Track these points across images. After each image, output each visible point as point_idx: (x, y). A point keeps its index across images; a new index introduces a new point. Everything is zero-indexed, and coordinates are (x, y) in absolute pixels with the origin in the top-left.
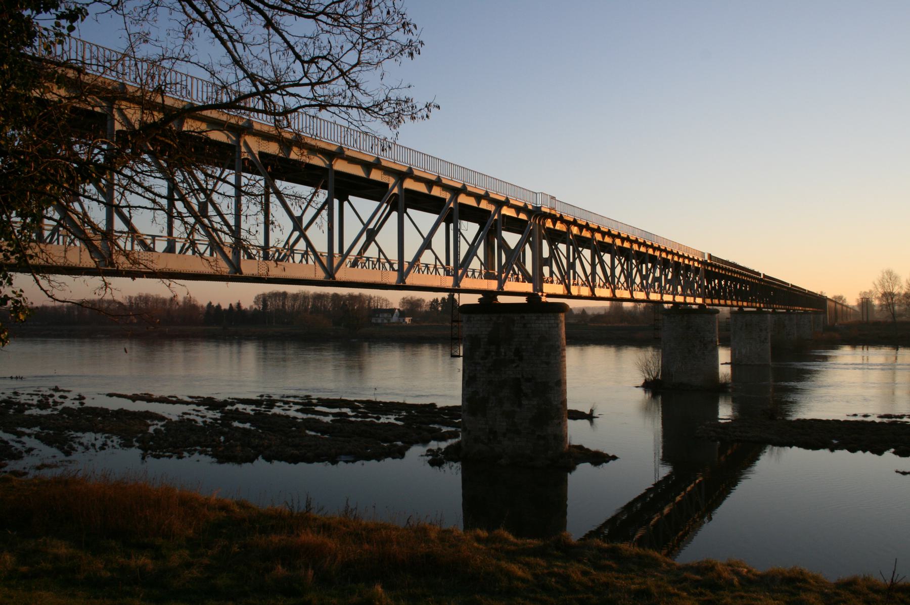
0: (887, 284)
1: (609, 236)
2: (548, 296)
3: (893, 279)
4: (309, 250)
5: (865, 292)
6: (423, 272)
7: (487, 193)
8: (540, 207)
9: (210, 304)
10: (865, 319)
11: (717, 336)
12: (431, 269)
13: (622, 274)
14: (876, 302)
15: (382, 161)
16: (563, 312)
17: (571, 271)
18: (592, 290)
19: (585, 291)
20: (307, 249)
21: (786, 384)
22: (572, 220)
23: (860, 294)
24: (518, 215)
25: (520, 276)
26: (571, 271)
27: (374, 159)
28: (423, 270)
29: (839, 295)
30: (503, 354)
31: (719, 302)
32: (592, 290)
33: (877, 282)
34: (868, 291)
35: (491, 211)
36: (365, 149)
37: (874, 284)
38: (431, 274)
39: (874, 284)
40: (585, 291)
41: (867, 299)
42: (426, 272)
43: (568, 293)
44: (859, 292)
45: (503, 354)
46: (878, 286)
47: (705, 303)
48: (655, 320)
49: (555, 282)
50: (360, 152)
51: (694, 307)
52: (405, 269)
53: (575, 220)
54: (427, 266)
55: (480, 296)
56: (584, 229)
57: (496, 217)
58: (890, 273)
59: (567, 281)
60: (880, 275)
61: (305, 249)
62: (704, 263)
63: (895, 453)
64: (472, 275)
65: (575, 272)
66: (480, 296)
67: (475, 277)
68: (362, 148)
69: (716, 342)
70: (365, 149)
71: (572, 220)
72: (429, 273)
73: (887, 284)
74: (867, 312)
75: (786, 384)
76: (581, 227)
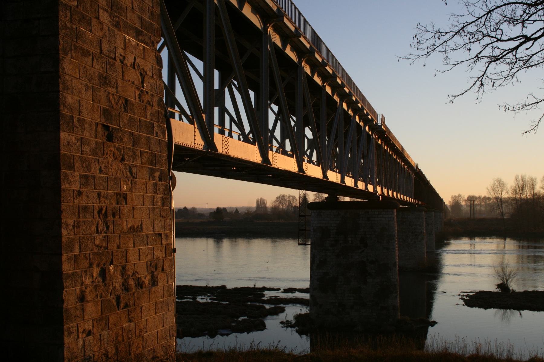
0: (497, 189)
3: (502, 186)
5: (455, 196)
10: (472, 217)
13: (233, 123)
14: (463, 203)
17: (216, 110)
21: (222, 302)
23: (452, 197)
26: (216, 110)
29: (283, 194)
30: (350, 242)
33: (490, 188)
34: (457, 195)
37: (488, 189)
39: (488, 189)
41: (457, 202)
44: (451, 196)
45: (350, 242)
46: (491, 191)
48: (300, 216)
58: (499, 181)
60: (492, 183)
63: (297, 331)
65: (223, 111)
73: (497, 189)
74: (474, 214)
75: (222, 302)
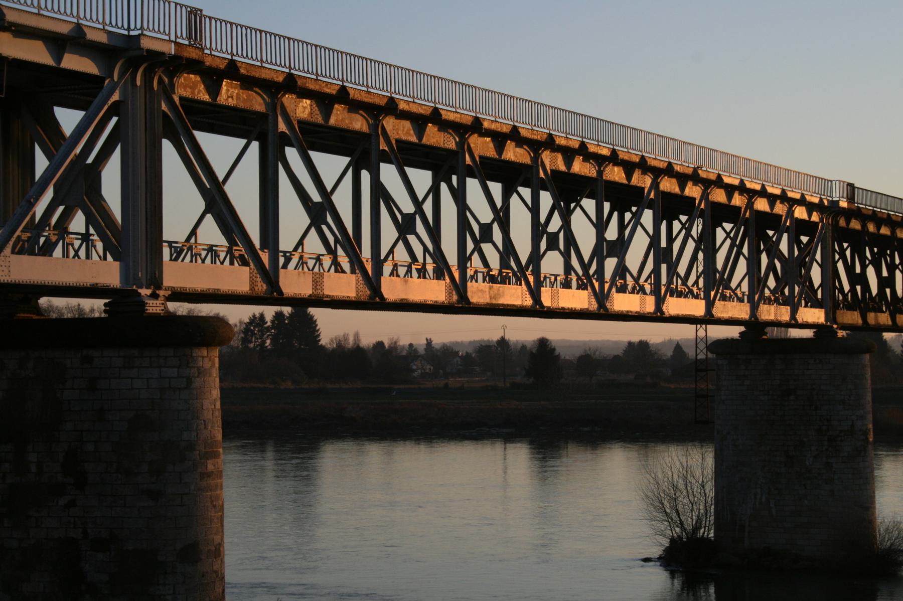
1: (741, 194)
2: (179, 295)
4: (92, 231)
6: (203, 261)
7: (436, 111)
8: (838, 202)
9: (429, 343)
11: (870, 417)
12: (222, 255)
15: (86, 30)
16: (208, 343)
18: (535, 294)
19: (579, 299)
20: (87, 229)
22: (577, 146)
24: (59, 58)
25: (430, 268)
27: (71, 26)
28: (203, 256)
30: (33, 468)
31: (864, 318)
32: (535, 294)
35: (643, 189)
36: (88, 17)
38: (222, 263)
40: (579, 299)
42: (82, 253)
43: (458, 302)
45: (33, 468)
47: (835, 321)
49: (574, 284)
50: (317, 80)
51: (795, 333)
52: (662, 294)
53: (614, 152)
54: (211, 249)
55: (742, 329)
56: (778, 202)
57: (702, 206)
59: (596, 285)
61: (84, 231)
62: (830, 209)
64: (407, 273)
66: (742, 329)
67: (398, 276)
68: (108, 22)
69: (866, 433)
70: (88, 17)
71: (577, 146)
72: (199, 261)
76: (811, 207)
